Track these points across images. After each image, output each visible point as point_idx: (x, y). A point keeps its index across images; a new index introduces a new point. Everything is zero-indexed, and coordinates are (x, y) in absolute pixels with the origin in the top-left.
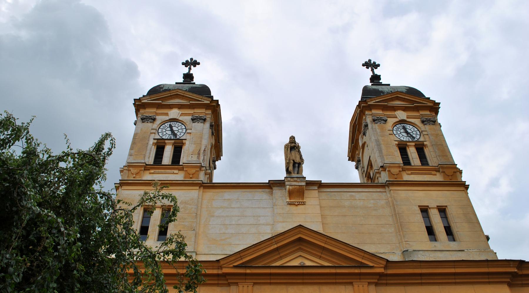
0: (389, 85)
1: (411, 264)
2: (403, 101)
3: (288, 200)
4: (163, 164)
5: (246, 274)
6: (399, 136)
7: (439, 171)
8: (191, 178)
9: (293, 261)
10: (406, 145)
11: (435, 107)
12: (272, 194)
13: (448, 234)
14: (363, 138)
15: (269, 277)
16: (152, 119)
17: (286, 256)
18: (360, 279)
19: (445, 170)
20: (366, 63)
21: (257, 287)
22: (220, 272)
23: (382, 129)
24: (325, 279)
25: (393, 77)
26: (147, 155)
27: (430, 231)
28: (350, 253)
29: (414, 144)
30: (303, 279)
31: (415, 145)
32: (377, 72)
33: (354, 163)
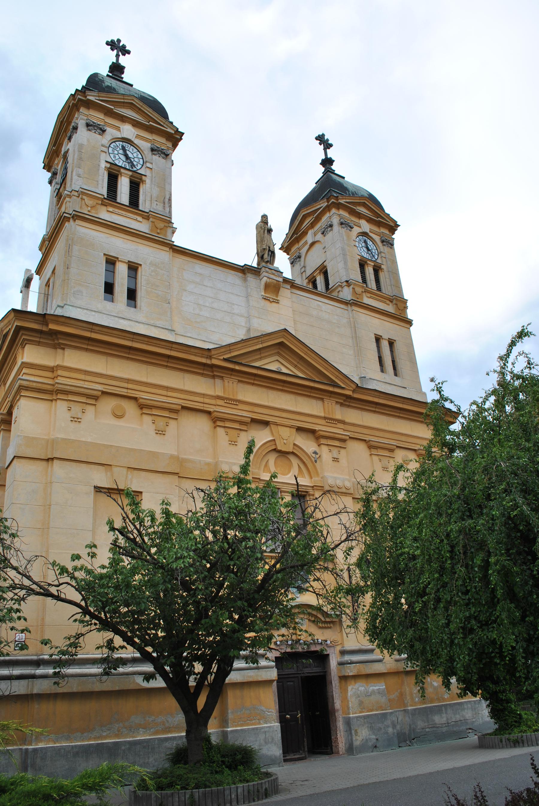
0: (132, 85)
1: (373, 393)
2: (137, 113)
3: (263, 294)
4: (118, 201)
5: (233, 370)
6: (115, 157)
7: (392, 302)
8: (158, 233)
9: (270, 364)
10: (366, 262)
11: (175, 137)
12: (245, 280)
13: (106, 291)
14: (68, 144)
15: (253, 378)
16: (101, 129)
17: (266, 357)
18: (330, 397)
19: (398, 303)
20: (112, 41)
21: (241, 385)
22: (208, 362)
23: (348, 237)
24: (247, 378)
25: (139, 76)
26: (100, 182)
27: (109, 288)
28: (325, 369)
29: (373, 264)
30: (283, 386)
31: (131, 176)
32: (123, 60)
33: (49, 175)
